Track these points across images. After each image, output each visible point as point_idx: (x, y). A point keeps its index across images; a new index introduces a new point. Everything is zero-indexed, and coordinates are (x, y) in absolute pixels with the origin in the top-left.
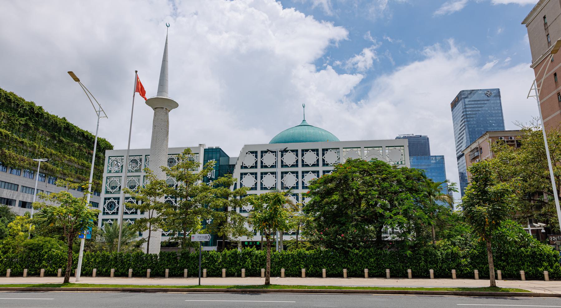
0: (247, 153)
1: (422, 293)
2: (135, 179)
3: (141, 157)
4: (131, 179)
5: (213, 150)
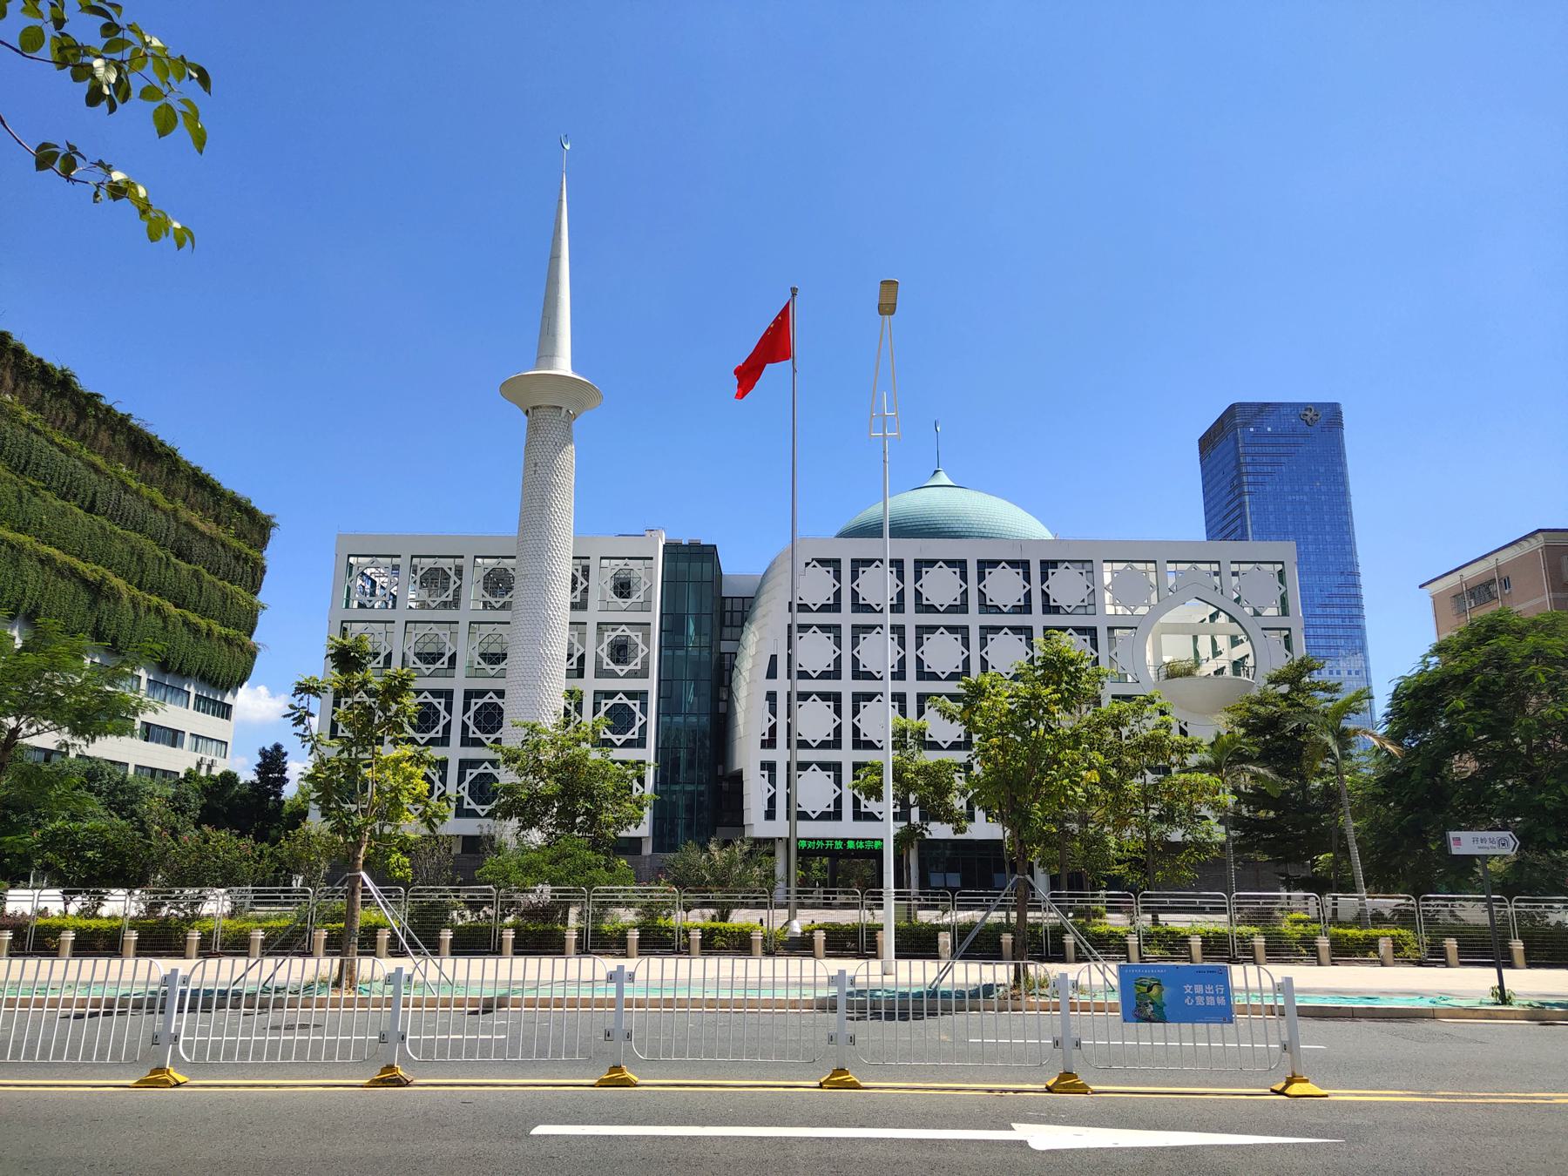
0: (807, 564)
1: (1352, 1014)
2: (632, 635)
3: (458, 561)
5: (680, 550)
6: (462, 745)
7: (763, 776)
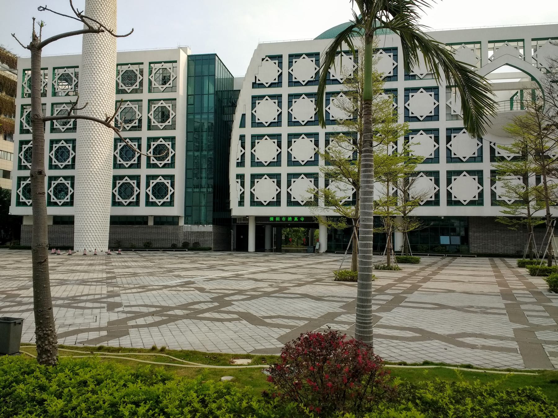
0: (263, 59)
2: (133, 106)
4: (62, 108)
6: (252, 166)
7: (238, 182)
